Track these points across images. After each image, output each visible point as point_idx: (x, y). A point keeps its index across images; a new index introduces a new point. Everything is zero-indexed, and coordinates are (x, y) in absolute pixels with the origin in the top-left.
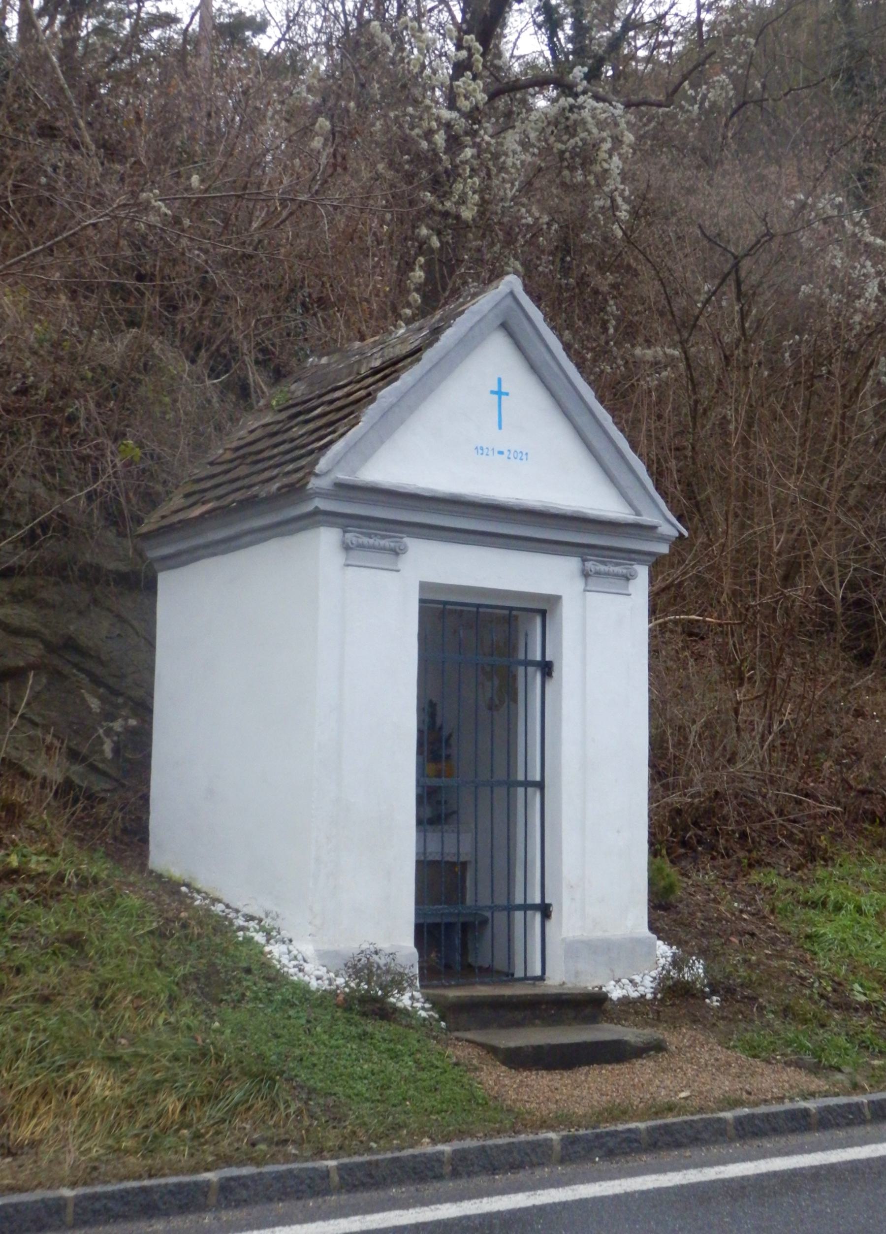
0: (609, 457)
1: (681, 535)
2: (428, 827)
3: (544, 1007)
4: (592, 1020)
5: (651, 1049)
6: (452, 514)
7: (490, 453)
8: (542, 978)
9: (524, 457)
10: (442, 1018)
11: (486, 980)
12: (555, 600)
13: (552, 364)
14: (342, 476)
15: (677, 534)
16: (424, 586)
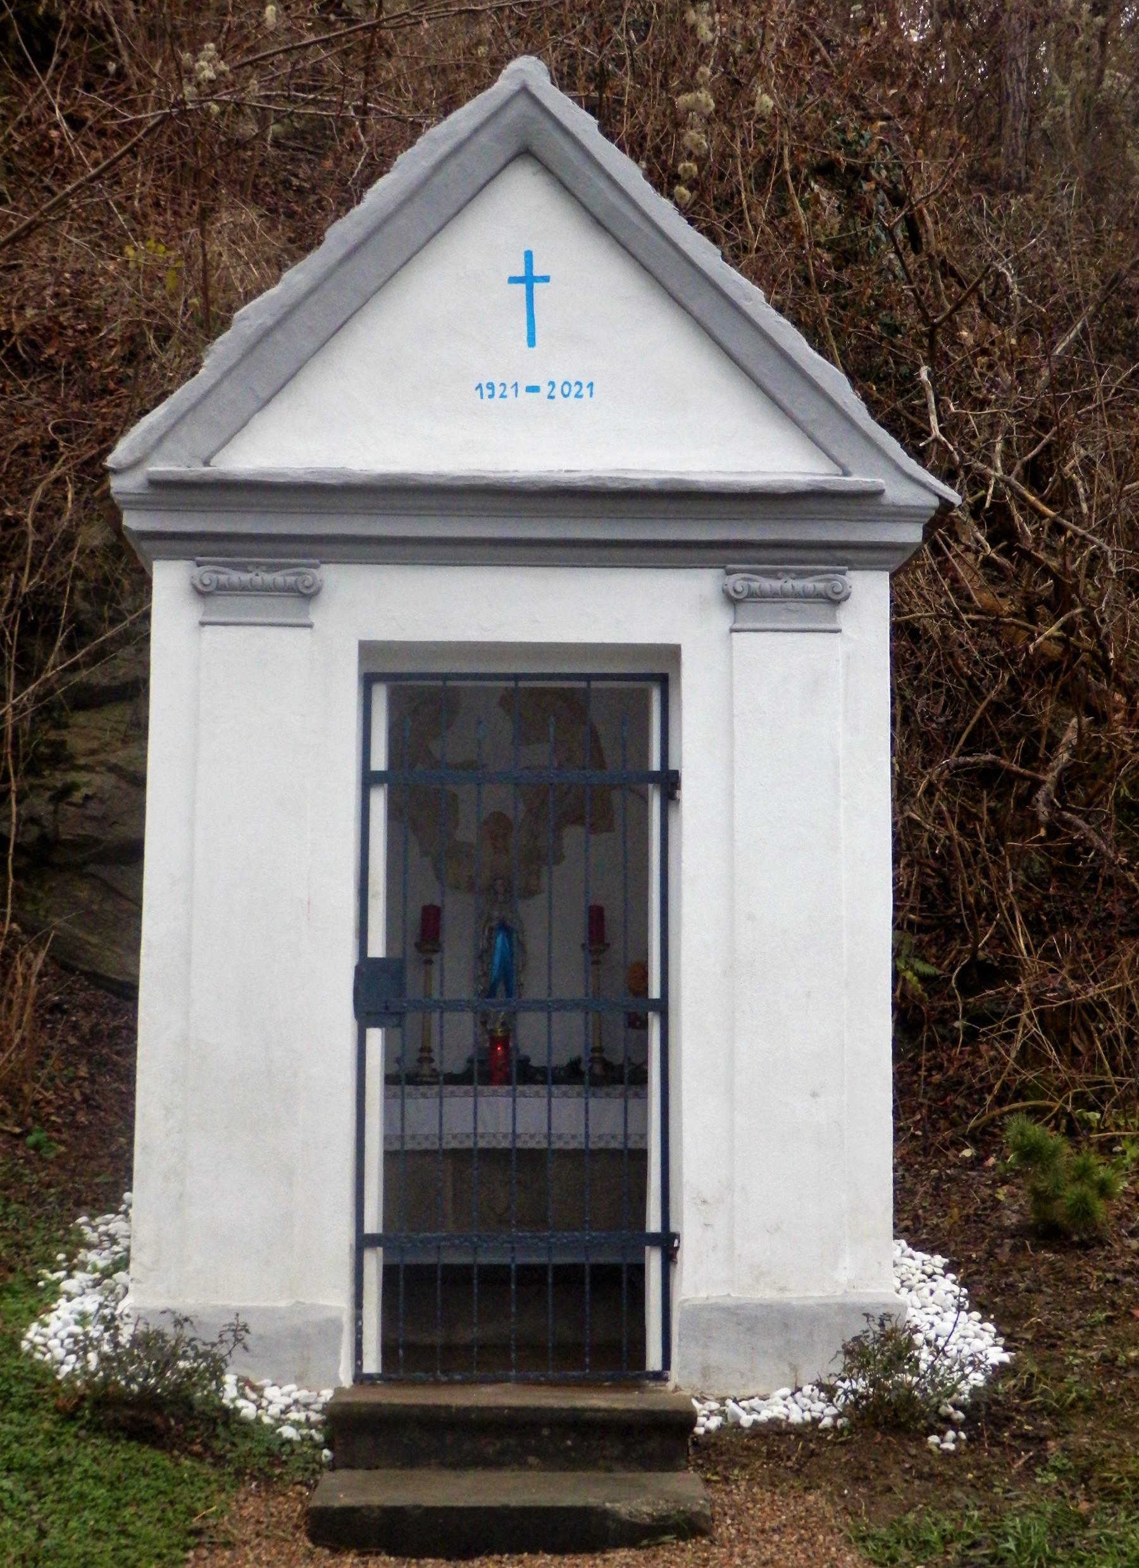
0: (767, 368)
1: (946, 506)
2: (409, 1089)
3: (545, 1432)
4: (668, 1462)
5: (665, 1531)
6: (220, 508)
7: (510, 392)
8: (660, 1377)
9: (585, 391)
10: (329, 1444)
11: (531, 1375)
12: (673, 653)
13: (626, 209)
14: (161, 467)
15: (935, 502)
16: (368, 650)
